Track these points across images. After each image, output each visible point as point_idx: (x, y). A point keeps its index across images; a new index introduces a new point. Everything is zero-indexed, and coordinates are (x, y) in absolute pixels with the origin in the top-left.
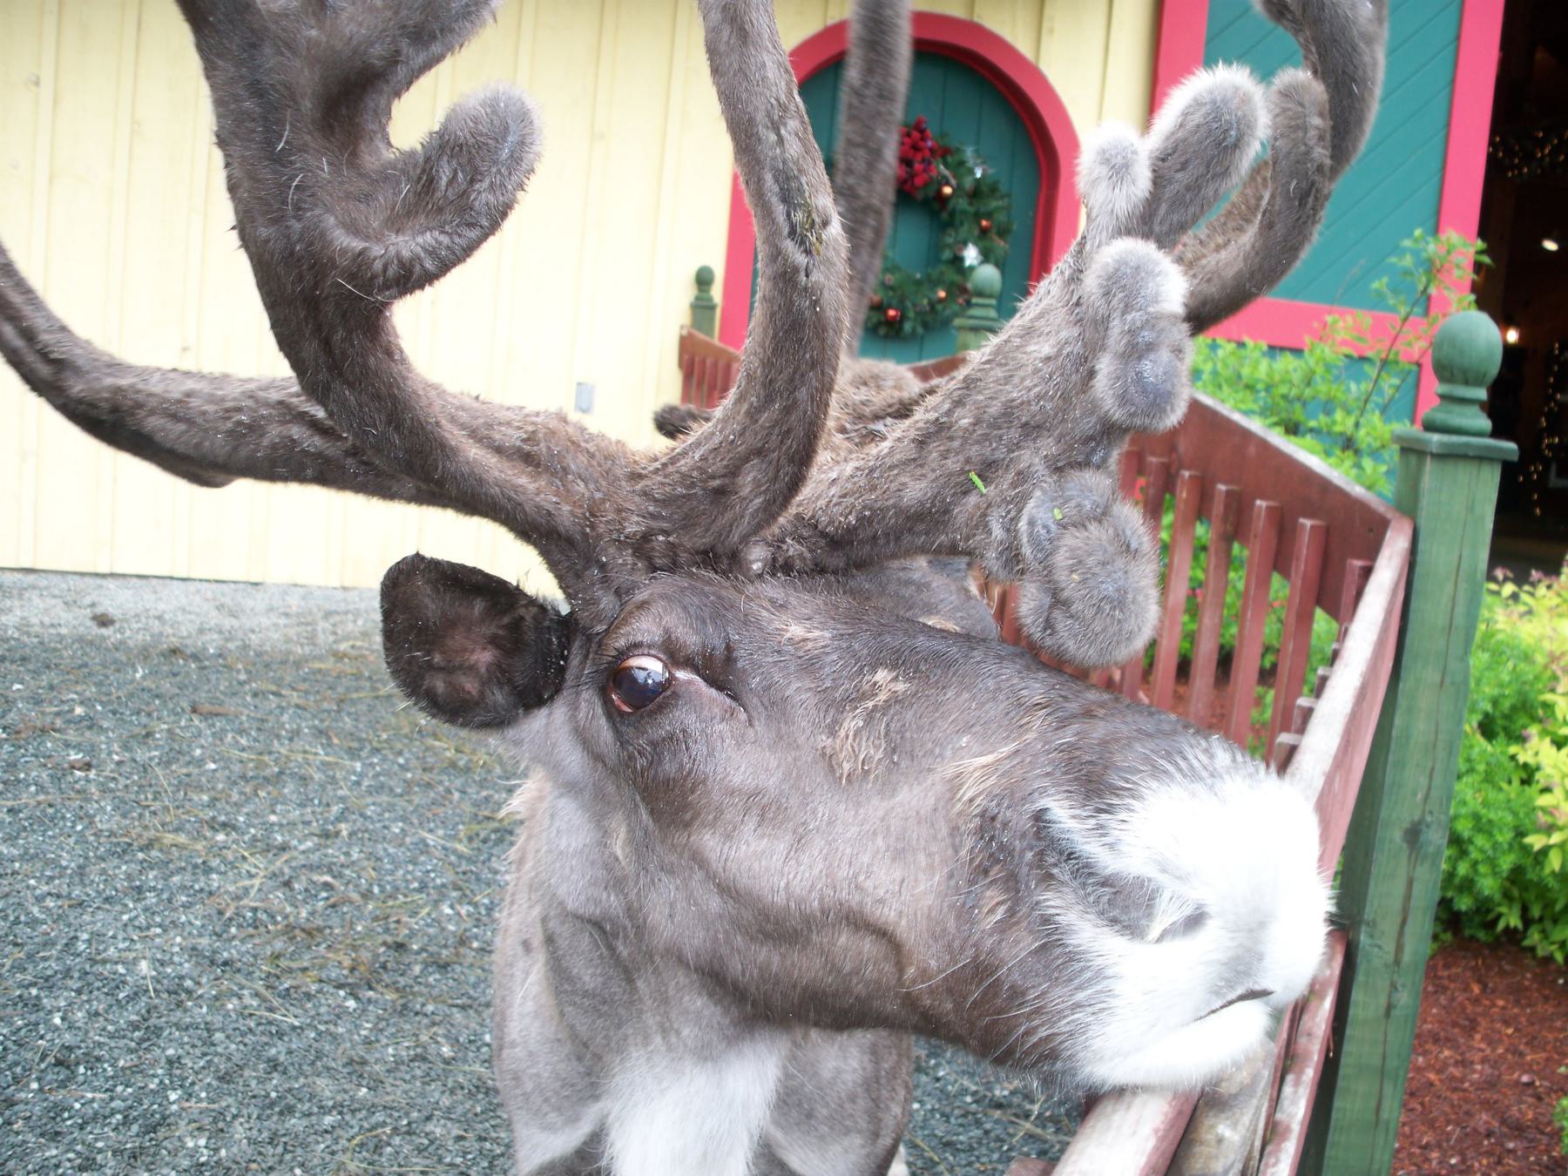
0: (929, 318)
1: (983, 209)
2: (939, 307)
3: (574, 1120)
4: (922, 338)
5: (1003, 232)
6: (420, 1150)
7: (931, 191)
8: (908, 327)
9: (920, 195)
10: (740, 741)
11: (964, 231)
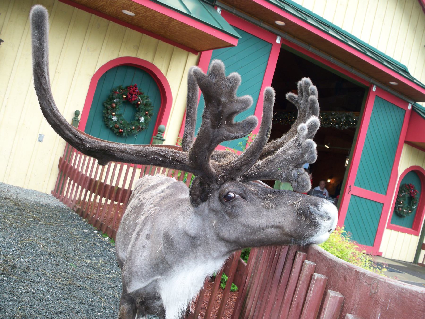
0: (130, 133)
1: (147, 109)
2: (133, 131)
3: (146, 281)
4: (126, 137)
5: (150, 115)
6: (34, 311)
7: (136, 102)
8: (124, 134)
9: (133, 103)
10: (247, 205)
11: (141, 113)
